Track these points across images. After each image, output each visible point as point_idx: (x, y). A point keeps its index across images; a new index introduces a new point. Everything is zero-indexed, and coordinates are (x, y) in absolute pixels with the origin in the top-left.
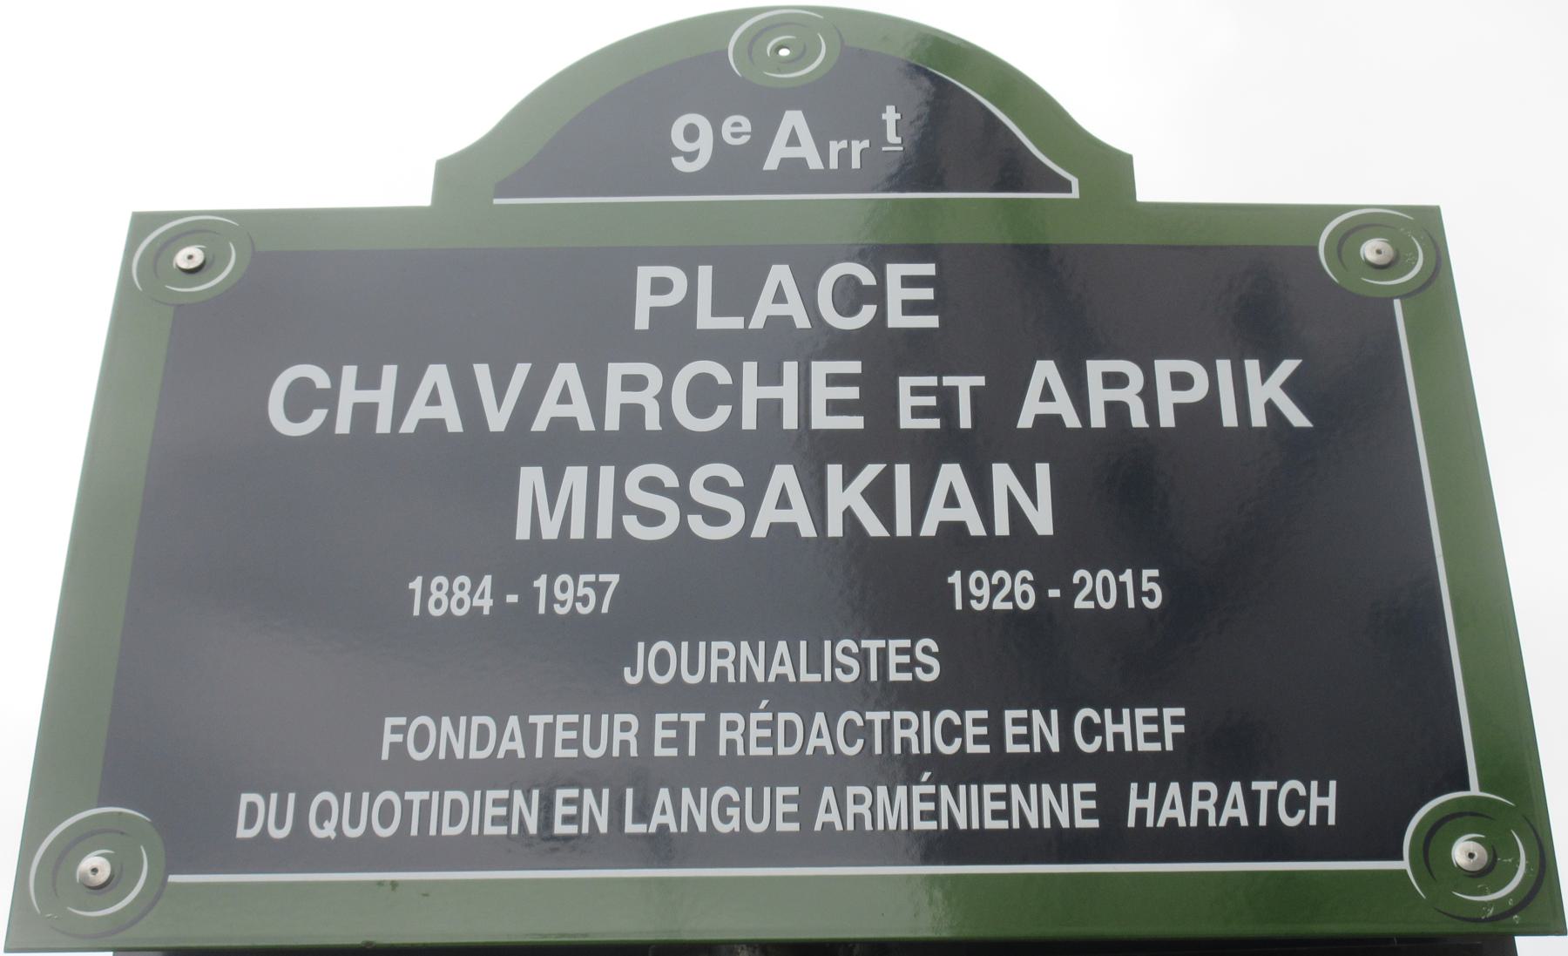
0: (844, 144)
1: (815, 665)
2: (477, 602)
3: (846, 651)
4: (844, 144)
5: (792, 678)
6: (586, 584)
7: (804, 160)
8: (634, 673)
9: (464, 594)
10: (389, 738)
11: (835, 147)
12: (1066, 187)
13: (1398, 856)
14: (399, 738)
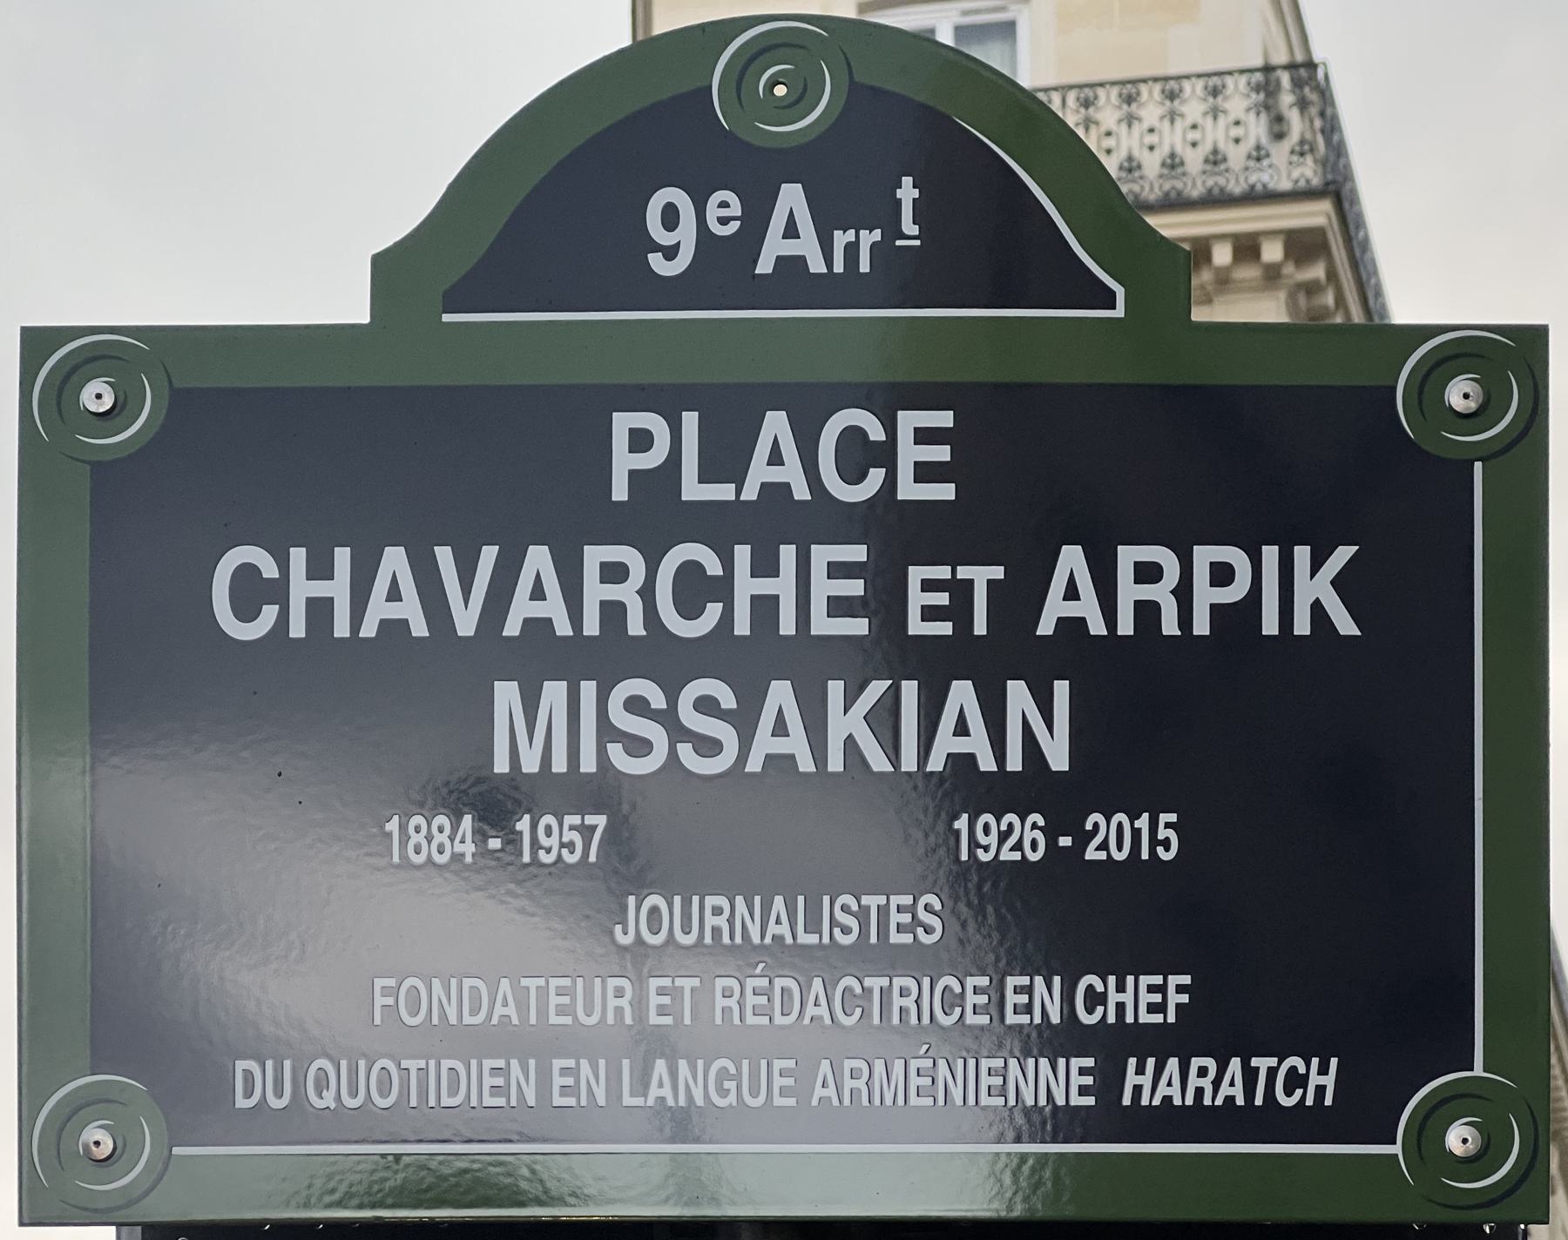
2: (458, 848)
11: (841, 239)
13: (1394, 1143)
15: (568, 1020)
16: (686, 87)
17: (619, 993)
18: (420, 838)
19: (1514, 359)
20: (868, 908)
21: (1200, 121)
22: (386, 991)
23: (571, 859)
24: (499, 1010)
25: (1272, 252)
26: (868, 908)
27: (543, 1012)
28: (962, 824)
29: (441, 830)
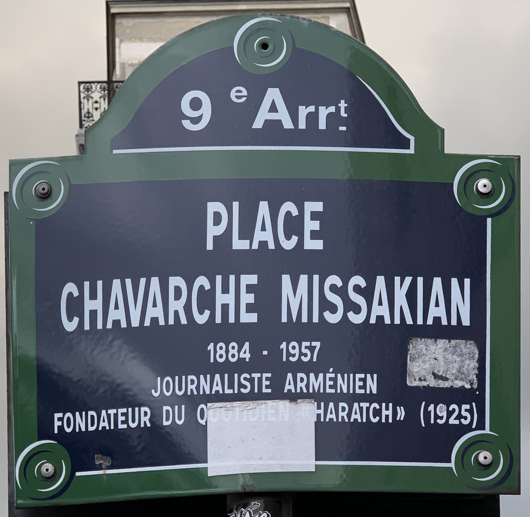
0: (312, 109)
1: (231, 386)
2: (242, 355)
3: (245, 379)
4: (312, 109)
5: (221, 392)
6: (306, 347)
8: (156, 392)
9: (235, 352)
10: (57, 424)
11: (303, 111)
13: (449, 461)
14: (60, 423)
16: (229, 45)
18: (223, 352)
19: (505, 169)
21: (98, 100)
23: (305, 359)
27: (116, 424)
29: (233, 348)
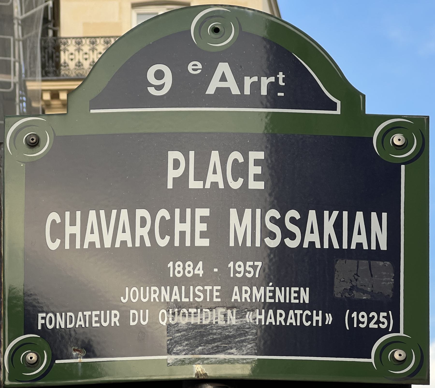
0: (255, 79)
1: (187, 296)
2: (196, 272)
3: (199, 290)
4: (255, 79)
7: (229, 89)
8: (124, 299)
9: (191, 269)
11: (248, 81)
12: (333, 107)
14: (43, 322)
15: (98, 325)
17: (116, 316)
18: (181, 269)
20: (207, 290)
22: (43, 318)
24: (78, 323)
25: (63, 96)
26: (207, 290)
27: (90, 323)
28: (231, 265)
